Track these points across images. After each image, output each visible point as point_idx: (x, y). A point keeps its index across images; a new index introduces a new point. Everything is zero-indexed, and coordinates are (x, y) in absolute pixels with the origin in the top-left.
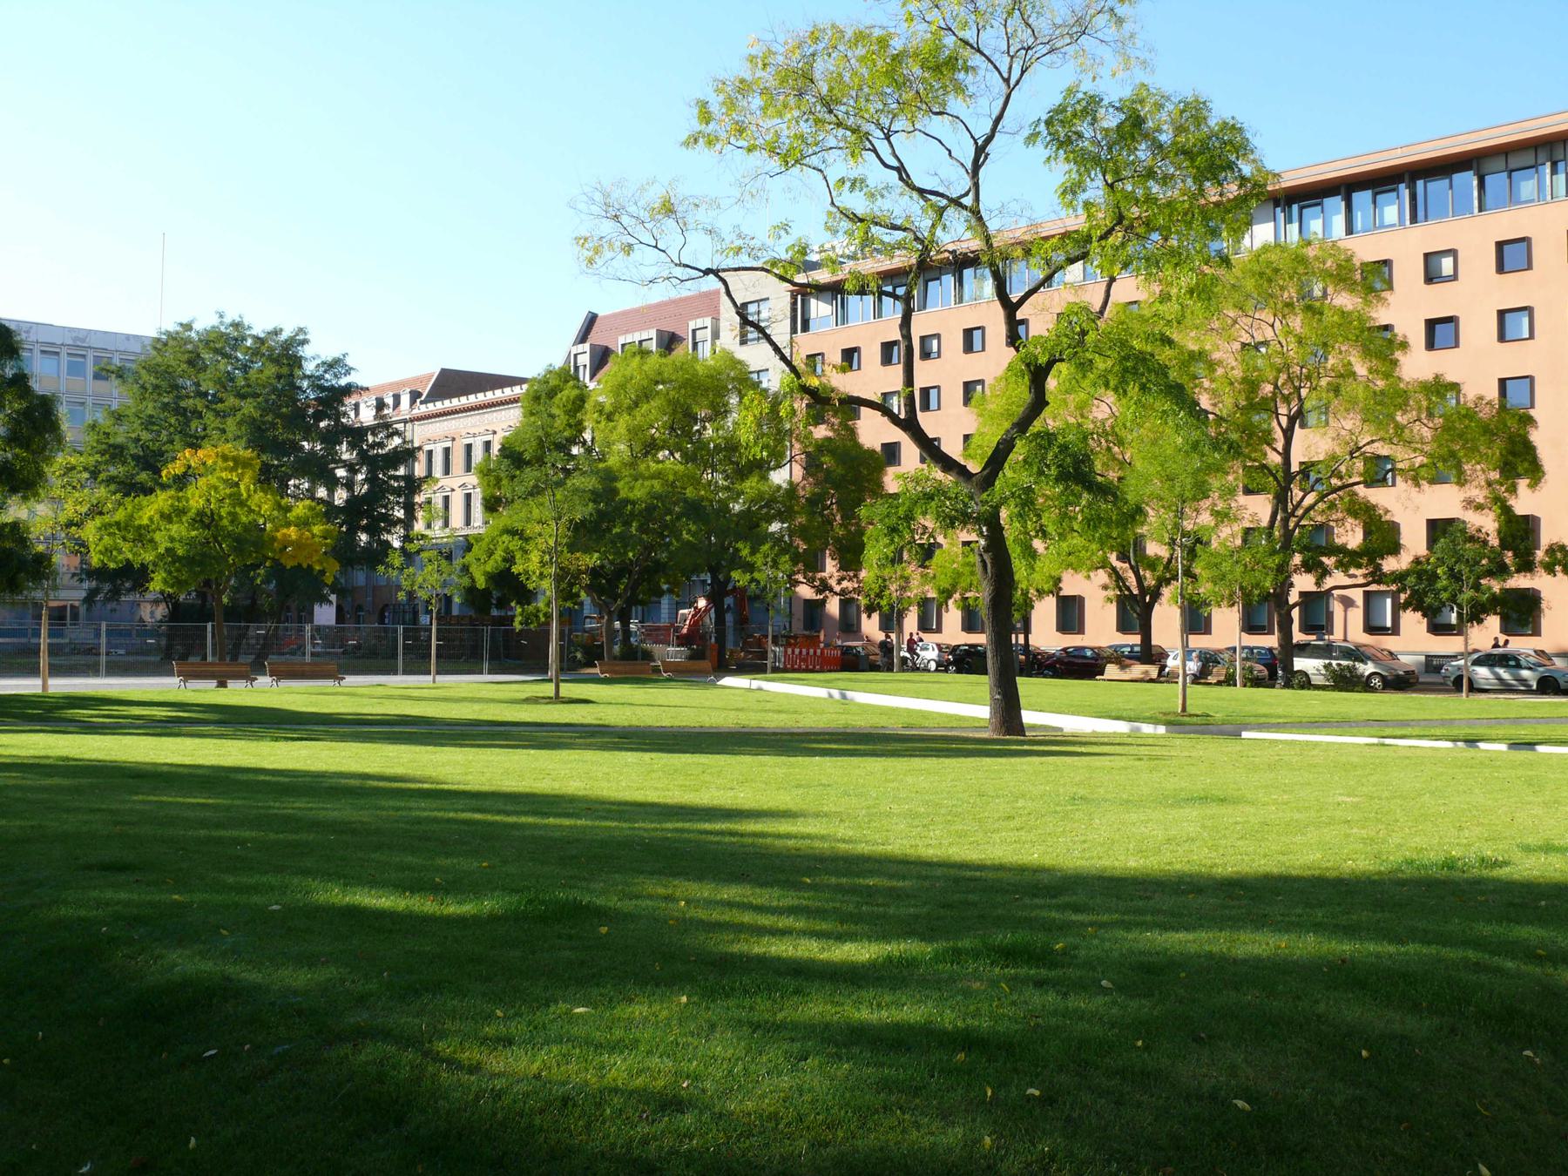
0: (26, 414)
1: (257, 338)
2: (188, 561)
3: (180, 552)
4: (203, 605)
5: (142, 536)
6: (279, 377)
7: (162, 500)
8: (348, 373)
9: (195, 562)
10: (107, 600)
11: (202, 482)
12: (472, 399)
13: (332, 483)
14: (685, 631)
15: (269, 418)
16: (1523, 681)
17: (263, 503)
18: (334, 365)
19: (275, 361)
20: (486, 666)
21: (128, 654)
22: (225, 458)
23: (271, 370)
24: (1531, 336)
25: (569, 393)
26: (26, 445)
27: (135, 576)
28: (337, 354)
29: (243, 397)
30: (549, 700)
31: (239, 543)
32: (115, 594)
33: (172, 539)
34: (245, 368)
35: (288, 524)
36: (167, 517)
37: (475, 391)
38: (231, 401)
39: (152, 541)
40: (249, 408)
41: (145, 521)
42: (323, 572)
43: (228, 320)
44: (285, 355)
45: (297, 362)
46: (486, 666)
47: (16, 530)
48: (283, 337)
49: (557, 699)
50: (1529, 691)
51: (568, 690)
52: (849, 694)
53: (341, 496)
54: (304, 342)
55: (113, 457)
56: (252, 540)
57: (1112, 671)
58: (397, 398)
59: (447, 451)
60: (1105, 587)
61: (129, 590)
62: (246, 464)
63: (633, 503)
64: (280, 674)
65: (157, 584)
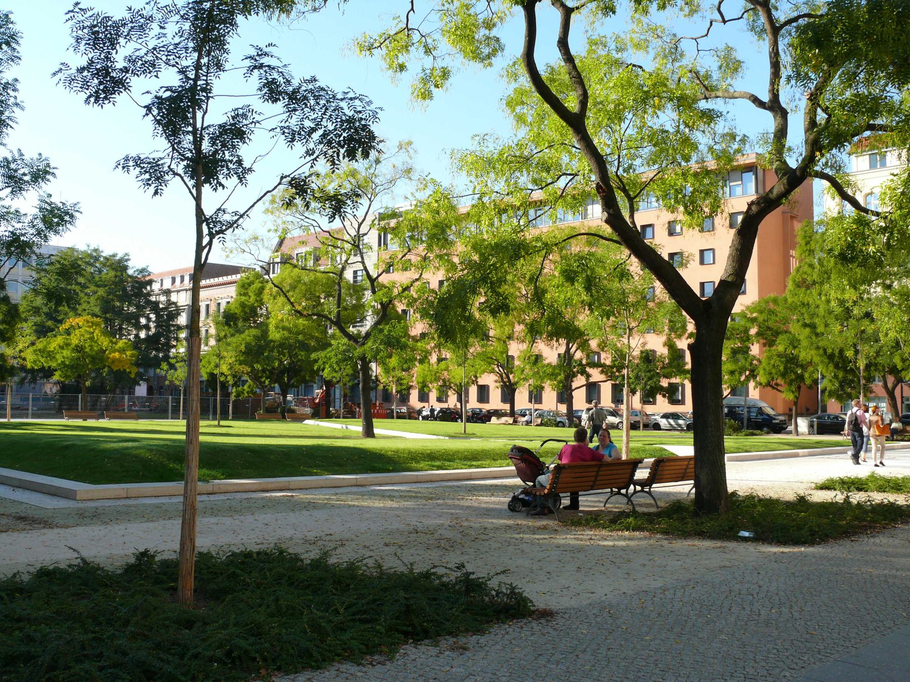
0: (9, 311)
1: (106, 258)
2: (71, 367)
3: (67, 363)
4: (78, 385)
5: (51, 355)
6: (116, 276)
7: (60, 340)
8: (149, 275)
9: (74, 367)
10: (30, 382)
11: (77, 332)
12: (221, 280)
13: (139, 327)
14: (317, 401)
15: (111, 297)
16: (679, 425)
17: (104, 342)
18: (142, 271)
19: (115, 270)
20: (211, 417)
21: (38, 410)
22: (88, 322)
23: (112, 273)
24: (714, 263)
25: (257, 285)
26: (8, 323)
27: (48, 373)
28: (144, 266)
29: (98, 286)
30: (215, 426)
31: (94, 359)
32: (34, 380)
33: (64, 357)
34: (100, 271)
35: (115, 351)
36: (62, 348)
37: (227, 275)
38: (93, 288)
39: (54, 357)
40: (101, 292)
41: (52, 349)
42: (130, 372)
43: (92, 248)
44: (119, 266)
45: (126, 268)
46: (211, 417)
47: (1, 357)
48: (117, 258)
49: (219, 426)
50: (682, 430)
51: (223, 423)
52: (349, 427)
53: (143, 335)
54: (127, 260)
55: (34, 313)
56: (99, 357)
57: (494, 419)
58: (182, 278)
59: (208, 306)
60: (496, 381)
61: (41, 378)
62: (97, 325)
63: (274, 342)
64: (112, 417)
65: (57, 377)
